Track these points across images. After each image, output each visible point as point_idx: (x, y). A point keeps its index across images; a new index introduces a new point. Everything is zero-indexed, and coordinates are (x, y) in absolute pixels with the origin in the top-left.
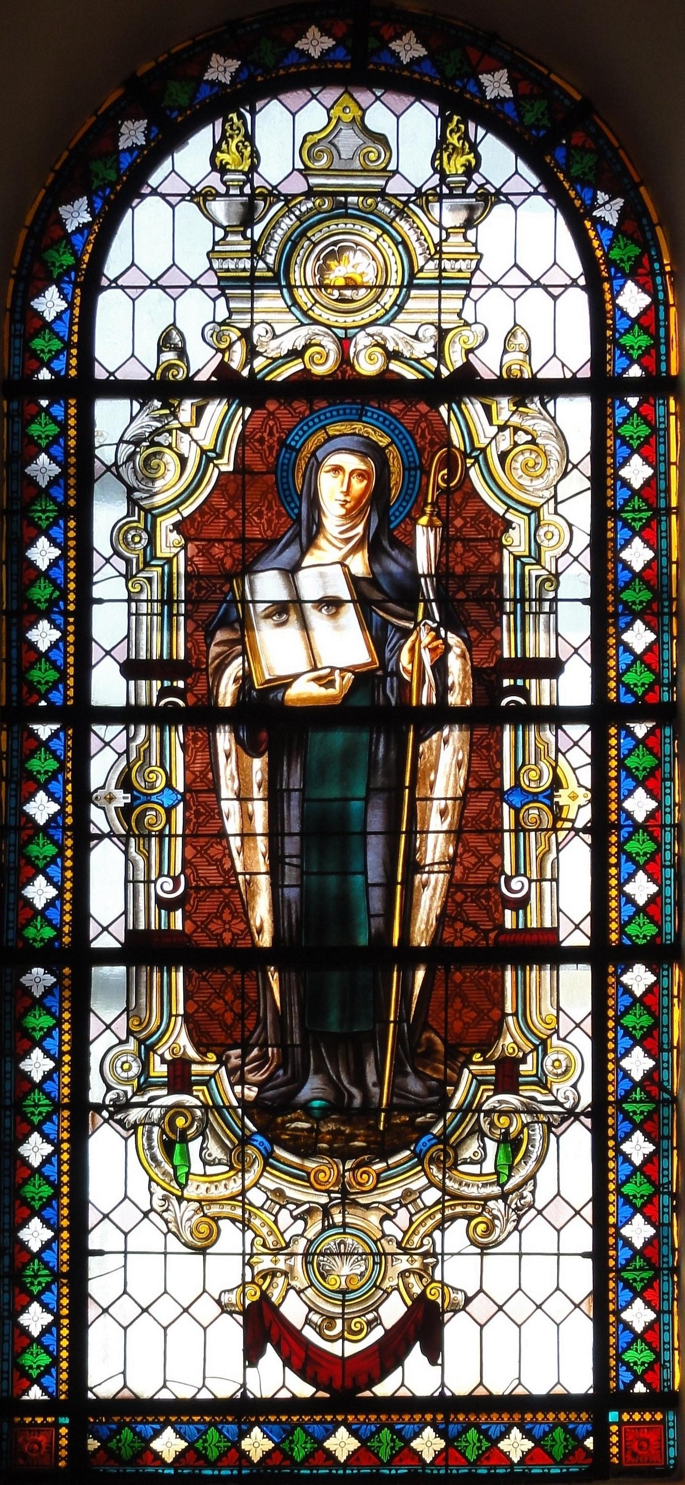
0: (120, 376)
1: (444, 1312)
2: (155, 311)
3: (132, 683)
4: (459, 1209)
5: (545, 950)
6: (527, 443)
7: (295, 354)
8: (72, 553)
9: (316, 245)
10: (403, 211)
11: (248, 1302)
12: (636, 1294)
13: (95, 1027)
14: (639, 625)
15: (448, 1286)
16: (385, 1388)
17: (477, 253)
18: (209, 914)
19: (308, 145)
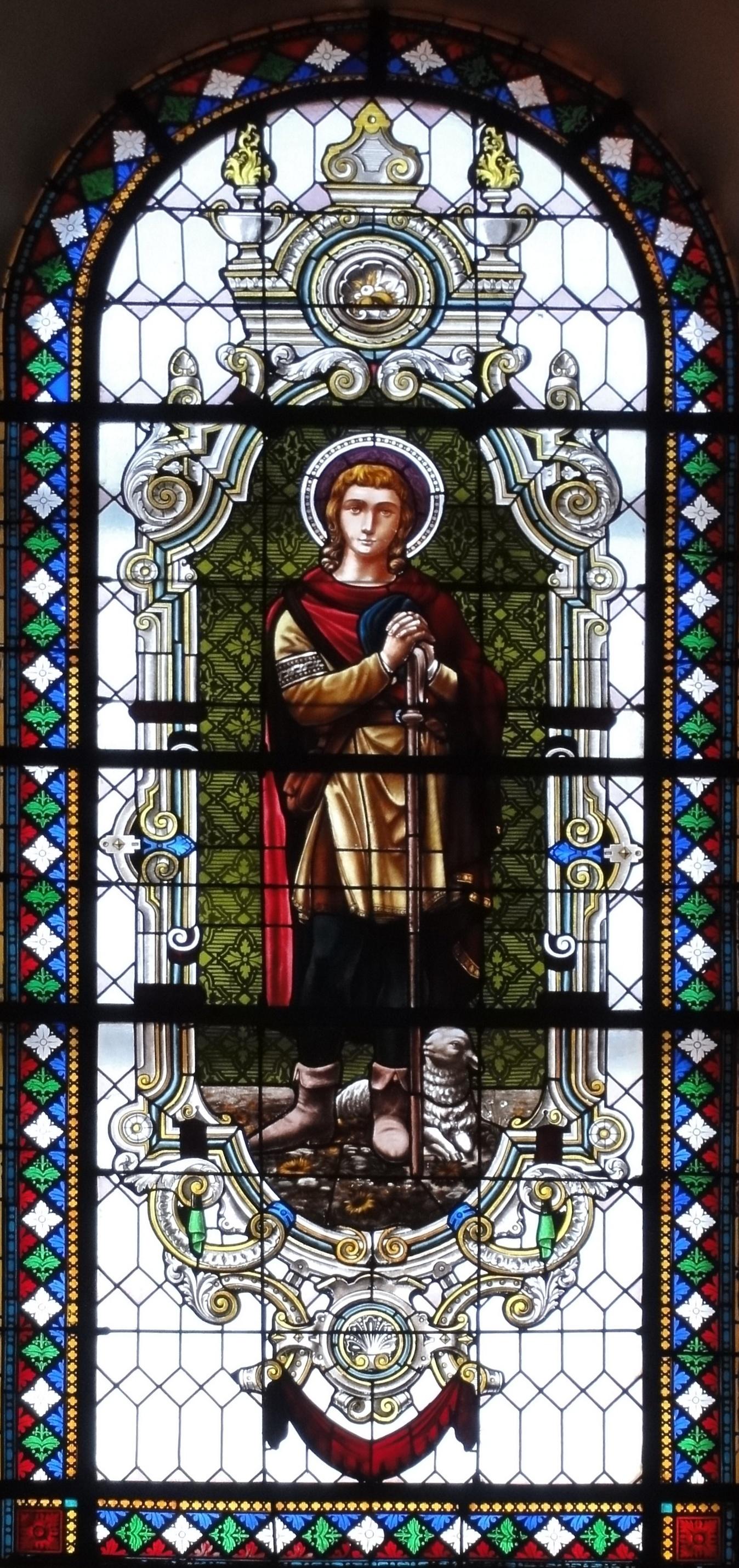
0: (127, 400)
1: (480, 1395)
2: (164, 331)
3: (141, 725)
4: (496, 1285)
5: (592, 1011)
6: (575, 479)
7: (320, 377)
8: (74, 1042)
9: (338, 262)
10: (437, 227)
11: (268, 1381)
12: (694, 1288)
13: (102, 1085)
14: (698, 673)
15: (484, 1368)
16: (414, 1475)
17: (520, 272)
18: (227, 945)
19: (329, 157)
